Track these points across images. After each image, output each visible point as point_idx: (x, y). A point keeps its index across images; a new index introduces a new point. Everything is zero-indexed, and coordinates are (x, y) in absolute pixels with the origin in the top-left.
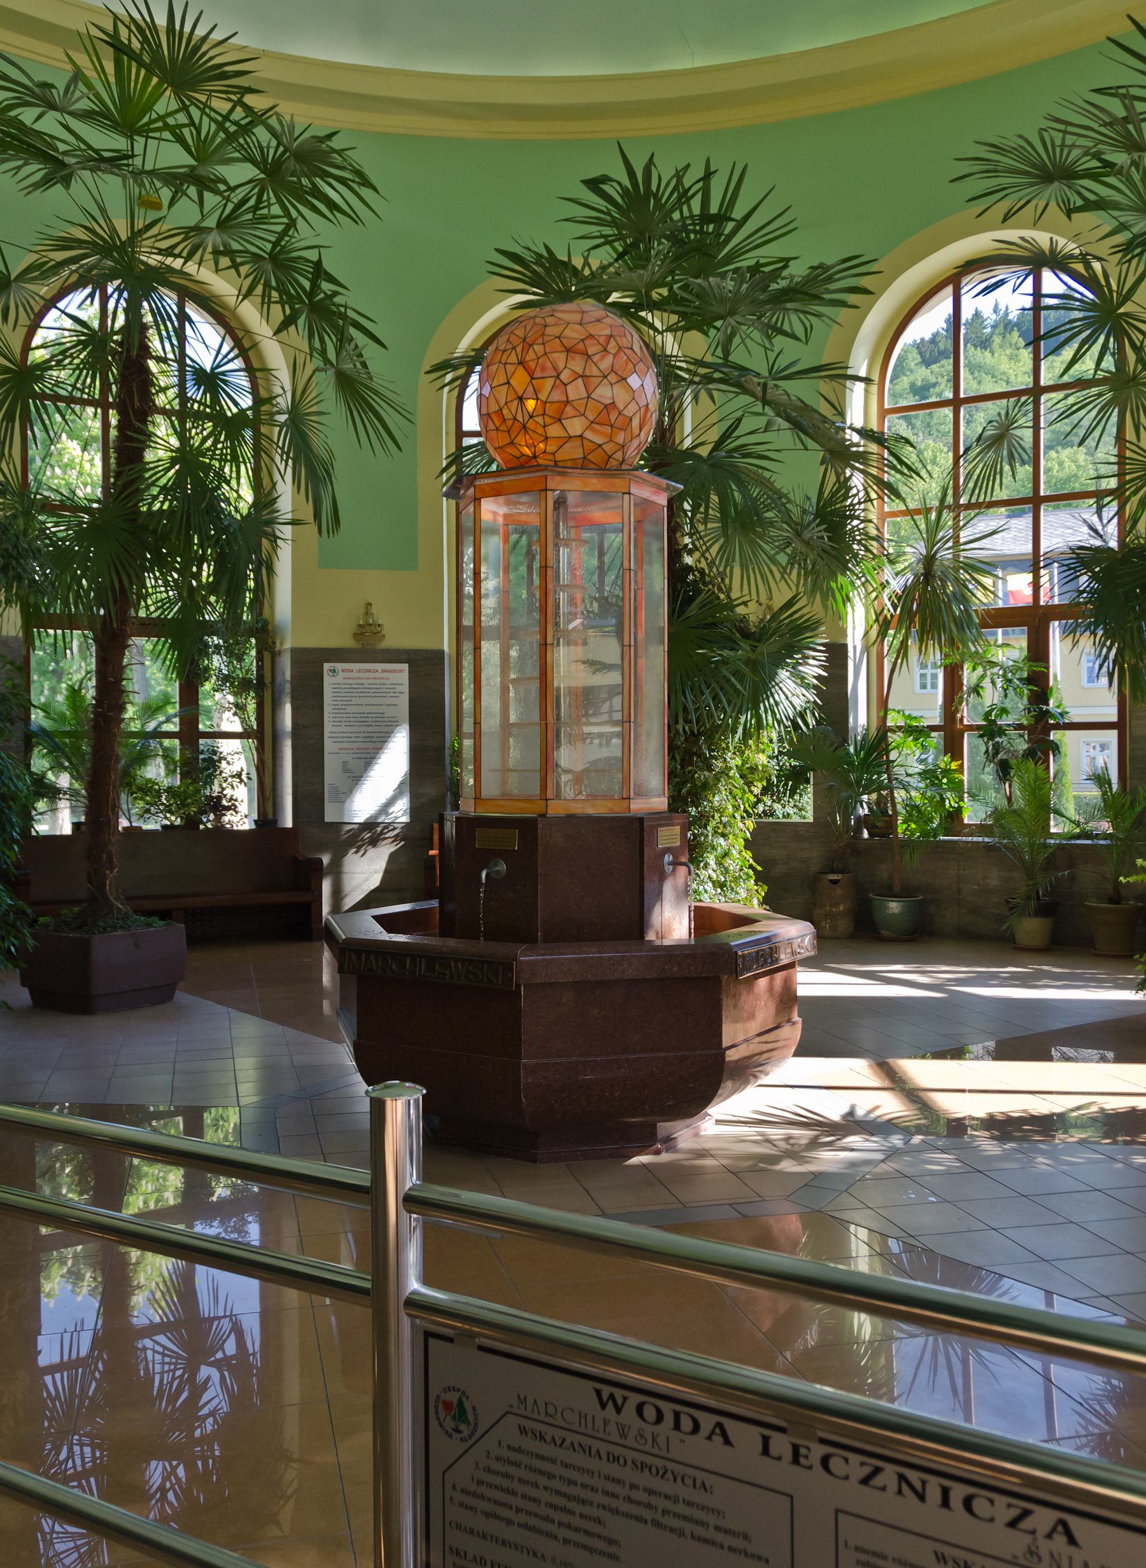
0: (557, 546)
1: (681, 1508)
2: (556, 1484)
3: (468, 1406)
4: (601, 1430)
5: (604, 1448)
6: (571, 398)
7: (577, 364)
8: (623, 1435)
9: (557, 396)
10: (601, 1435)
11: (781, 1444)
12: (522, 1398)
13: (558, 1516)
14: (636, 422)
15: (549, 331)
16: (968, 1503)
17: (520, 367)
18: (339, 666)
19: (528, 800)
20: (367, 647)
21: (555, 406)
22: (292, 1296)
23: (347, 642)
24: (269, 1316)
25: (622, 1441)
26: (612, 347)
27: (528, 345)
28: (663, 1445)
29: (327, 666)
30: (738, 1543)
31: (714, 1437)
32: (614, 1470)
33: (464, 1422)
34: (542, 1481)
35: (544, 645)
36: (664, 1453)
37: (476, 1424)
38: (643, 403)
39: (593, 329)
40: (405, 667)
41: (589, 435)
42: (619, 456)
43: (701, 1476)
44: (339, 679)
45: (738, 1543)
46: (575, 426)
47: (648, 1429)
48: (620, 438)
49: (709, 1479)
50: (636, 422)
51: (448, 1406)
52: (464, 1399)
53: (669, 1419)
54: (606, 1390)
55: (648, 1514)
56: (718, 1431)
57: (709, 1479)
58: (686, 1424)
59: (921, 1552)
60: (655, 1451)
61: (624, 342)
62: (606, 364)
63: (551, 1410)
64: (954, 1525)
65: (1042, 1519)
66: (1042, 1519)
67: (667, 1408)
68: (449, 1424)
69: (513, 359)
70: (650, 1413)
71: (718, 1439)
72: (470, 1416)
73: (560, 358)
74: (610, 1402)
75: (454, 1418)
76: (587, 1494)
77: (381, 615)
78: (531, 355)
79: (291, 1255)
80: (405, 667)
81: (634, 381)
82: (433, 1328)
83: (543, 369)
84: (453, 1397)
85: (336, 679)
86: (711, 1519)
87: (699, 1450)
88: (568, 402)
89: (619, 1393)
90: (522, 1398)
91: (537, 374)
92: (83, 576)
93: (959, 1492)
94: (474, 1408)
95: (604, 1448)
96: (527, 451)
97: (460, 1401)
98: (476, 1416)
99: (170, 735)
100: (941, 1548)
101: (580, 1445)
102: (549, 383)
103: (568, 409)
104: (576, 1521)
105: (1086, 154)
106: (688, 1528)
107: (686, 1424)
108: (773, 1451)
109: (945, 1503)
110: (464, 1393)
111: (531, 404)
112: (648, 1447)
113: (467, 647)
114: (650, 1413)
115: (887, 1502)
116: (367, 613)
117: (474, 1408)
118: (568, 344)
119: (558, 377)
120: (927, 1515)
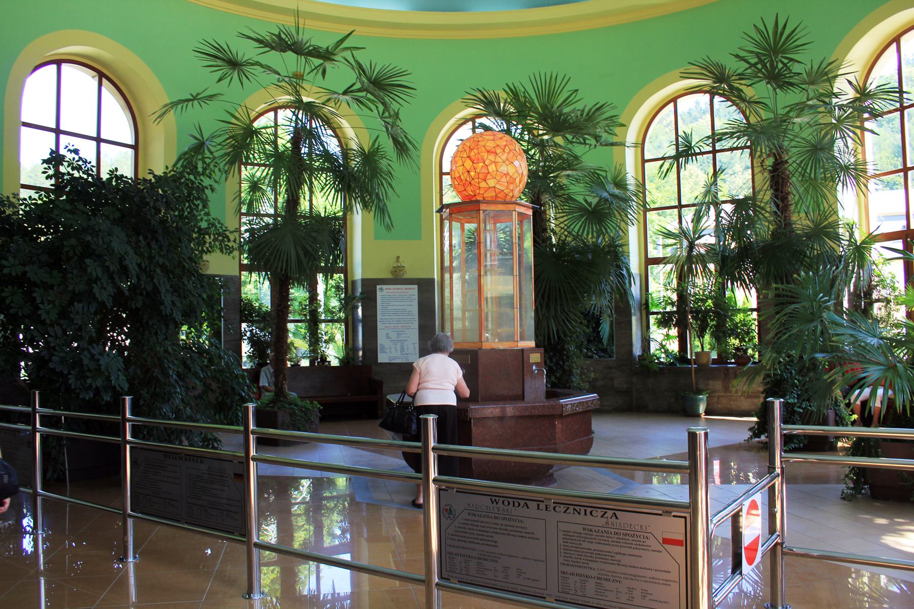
0: (485, 233)
1: (515, 529)
2: (479, 528)
5: (493, 515)
7: (492, 157)
11: (542, 506)
13: (481, 537)
14: (518, 180)
15: (480, 143)
16: (591, 513)
18: (384, 287)
19: (474, 343)
20: (397, 278)
22: (365, 576)
23: (389, 276)
24: (354, 583)
26: (507, 150)
29: (378, 287)
30: (531, 536)
32: (496, 521)
34: (475, 528)
35: (480, 276)
38: (520, 172)
39: (499, 142)
40: (416, 286)
41: (497, 186)
42: (511, 194)
44: (384, 293)
45: (531, 536)
46: (492, 183)
47: (506, 508)
48: (511, 187)
49: (523, 519)
50: (518, 180)
51: (446, 510)
53: (511, 504)
54: (493, 498)
55: (505, 532)
57: (523, 519)
58: (516, 504)
61: (512, 147)
62: (504, 157)
64: (588, 520)
65: (610, 513)
66: (610, 513)
67: (511, 501)
68: (447, 516)
69: (465, 155)
70: (506, 503)
73: (485, 155)
76: (488, 529)
77: (404, 262)
78: (472, 154)
79: (364, 562)
80: (416, 286)
81: (516, 163)
84: (448, 507)
85: (383, 293)
86: (524, 530)
87: (521, 511)
89: (497, 499)
92: (67, 194)
93: (589, 510)
95: (493, 515)
96: (471, 193)
99: (324, 321)
104: (485, 538)
106: (517, 534)
107: (516, 504)
111: (472, 174)
113: (447, 276)
114: (506, 503)
115: (572, 517)
118: (488, 149)
120: (581, 518)
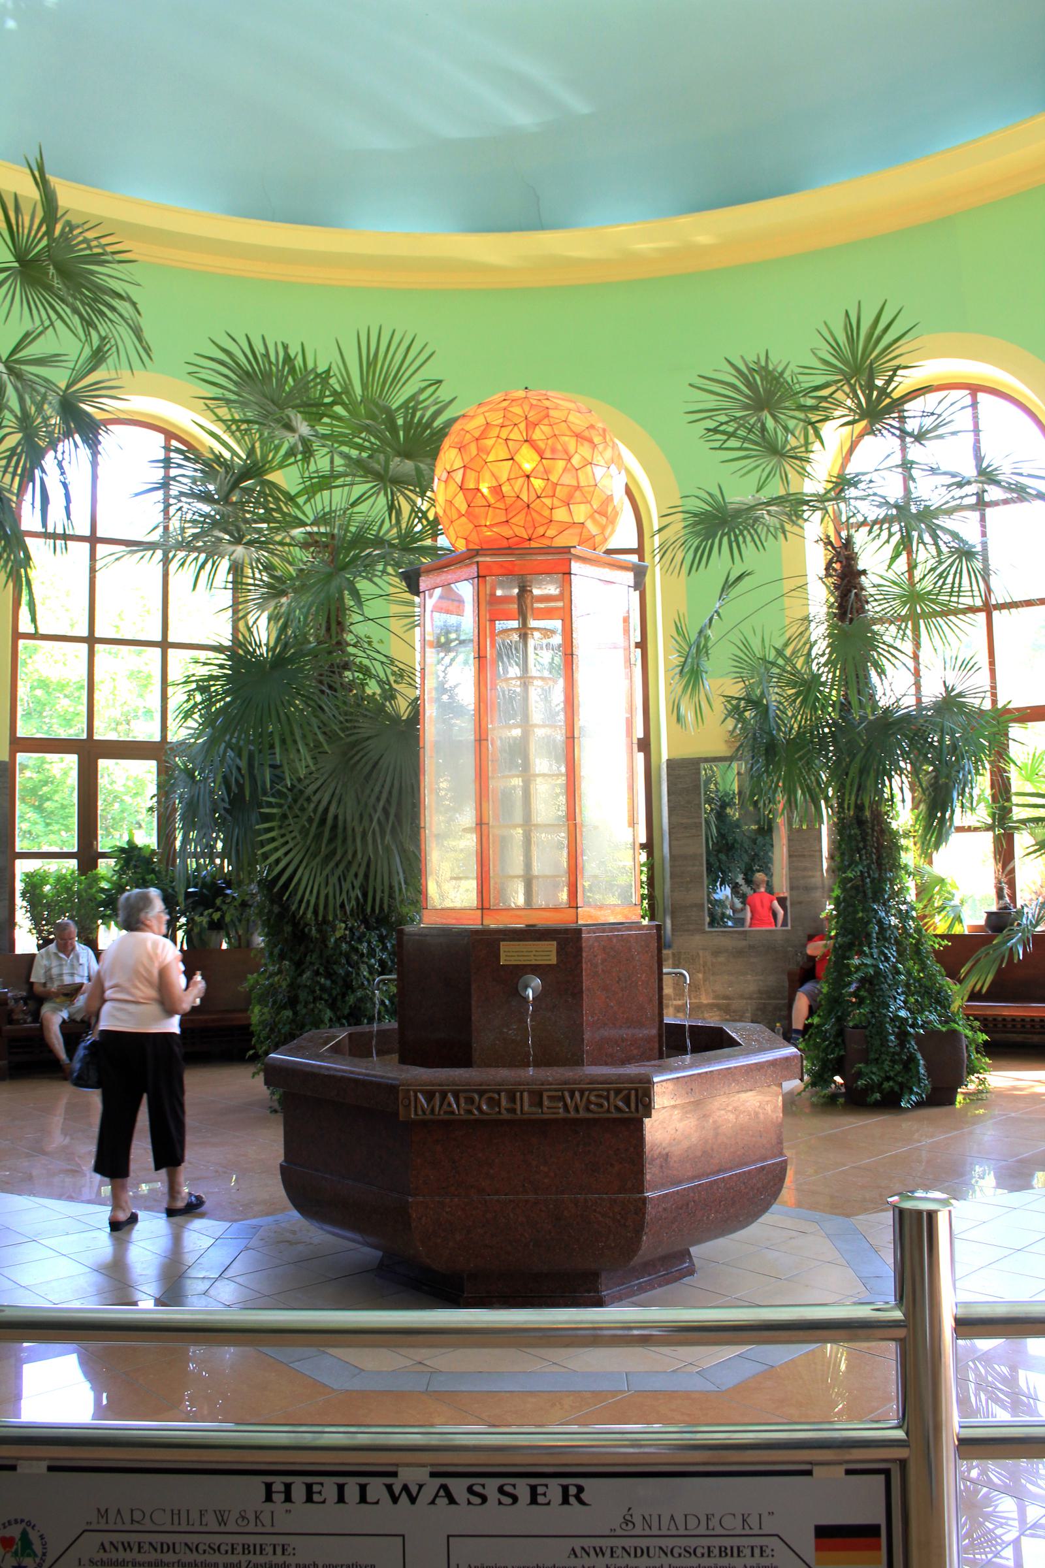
3: (33, 1536)
4: (197, 1522)
6: (582, 484)
8: (222, 1521)
9: (568, 480)
10: (197, 1528)
12: (103, 1511)
17: (526, 445)
21: (566, 489)
25: (222, 1529)
27: (531, 425)
28: (267, 1521)
31: (438, 1501)
33: (29, 1555)
36: (269, 1529)
37: (44, 1554)
41: (589, 524)
43: (605, 1543)
52: (29, 1529)
56: (442, 1493)
59: (558, 1552)
60: (260, 1529)
63: (137, 1516)
71: (442, 1501)
72: (37, 1547)
73: (571, 443)
74: (404, 1495)
75: (16, 1554)
82: (893, 1473)
83: (553, 450)
84: (15, 1532)
88: (578, 487)
90: (103, 1511)
91: (548, 455)
94: (42, 1537)
97: (24, 1534)
98: (44, 1545)
100: (577, 1543)
101: (111, 1543)
102: (561, 464)
103: (578, 494)
105: (102, 339)
108: (370, 1497)
109: (341, 1499)
110: (29, 1523)
112: (251, 1528)
116: (455, 687)
117: (42, 1537)
119: (569, 460)
